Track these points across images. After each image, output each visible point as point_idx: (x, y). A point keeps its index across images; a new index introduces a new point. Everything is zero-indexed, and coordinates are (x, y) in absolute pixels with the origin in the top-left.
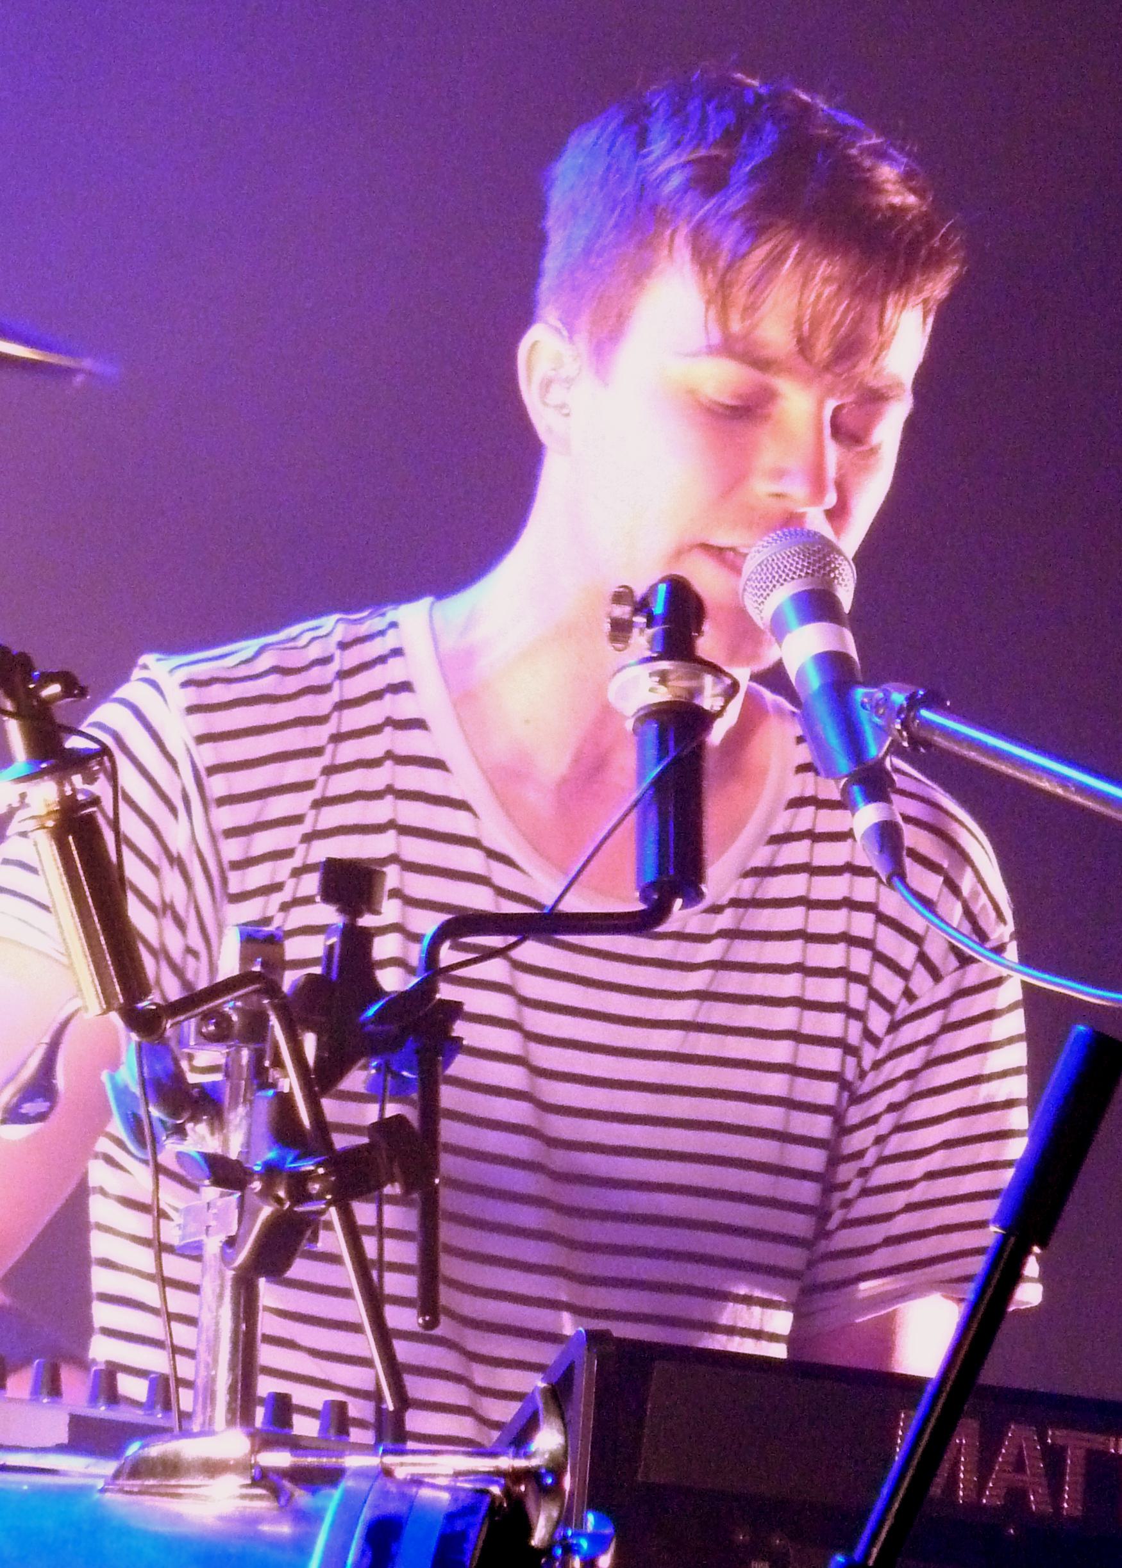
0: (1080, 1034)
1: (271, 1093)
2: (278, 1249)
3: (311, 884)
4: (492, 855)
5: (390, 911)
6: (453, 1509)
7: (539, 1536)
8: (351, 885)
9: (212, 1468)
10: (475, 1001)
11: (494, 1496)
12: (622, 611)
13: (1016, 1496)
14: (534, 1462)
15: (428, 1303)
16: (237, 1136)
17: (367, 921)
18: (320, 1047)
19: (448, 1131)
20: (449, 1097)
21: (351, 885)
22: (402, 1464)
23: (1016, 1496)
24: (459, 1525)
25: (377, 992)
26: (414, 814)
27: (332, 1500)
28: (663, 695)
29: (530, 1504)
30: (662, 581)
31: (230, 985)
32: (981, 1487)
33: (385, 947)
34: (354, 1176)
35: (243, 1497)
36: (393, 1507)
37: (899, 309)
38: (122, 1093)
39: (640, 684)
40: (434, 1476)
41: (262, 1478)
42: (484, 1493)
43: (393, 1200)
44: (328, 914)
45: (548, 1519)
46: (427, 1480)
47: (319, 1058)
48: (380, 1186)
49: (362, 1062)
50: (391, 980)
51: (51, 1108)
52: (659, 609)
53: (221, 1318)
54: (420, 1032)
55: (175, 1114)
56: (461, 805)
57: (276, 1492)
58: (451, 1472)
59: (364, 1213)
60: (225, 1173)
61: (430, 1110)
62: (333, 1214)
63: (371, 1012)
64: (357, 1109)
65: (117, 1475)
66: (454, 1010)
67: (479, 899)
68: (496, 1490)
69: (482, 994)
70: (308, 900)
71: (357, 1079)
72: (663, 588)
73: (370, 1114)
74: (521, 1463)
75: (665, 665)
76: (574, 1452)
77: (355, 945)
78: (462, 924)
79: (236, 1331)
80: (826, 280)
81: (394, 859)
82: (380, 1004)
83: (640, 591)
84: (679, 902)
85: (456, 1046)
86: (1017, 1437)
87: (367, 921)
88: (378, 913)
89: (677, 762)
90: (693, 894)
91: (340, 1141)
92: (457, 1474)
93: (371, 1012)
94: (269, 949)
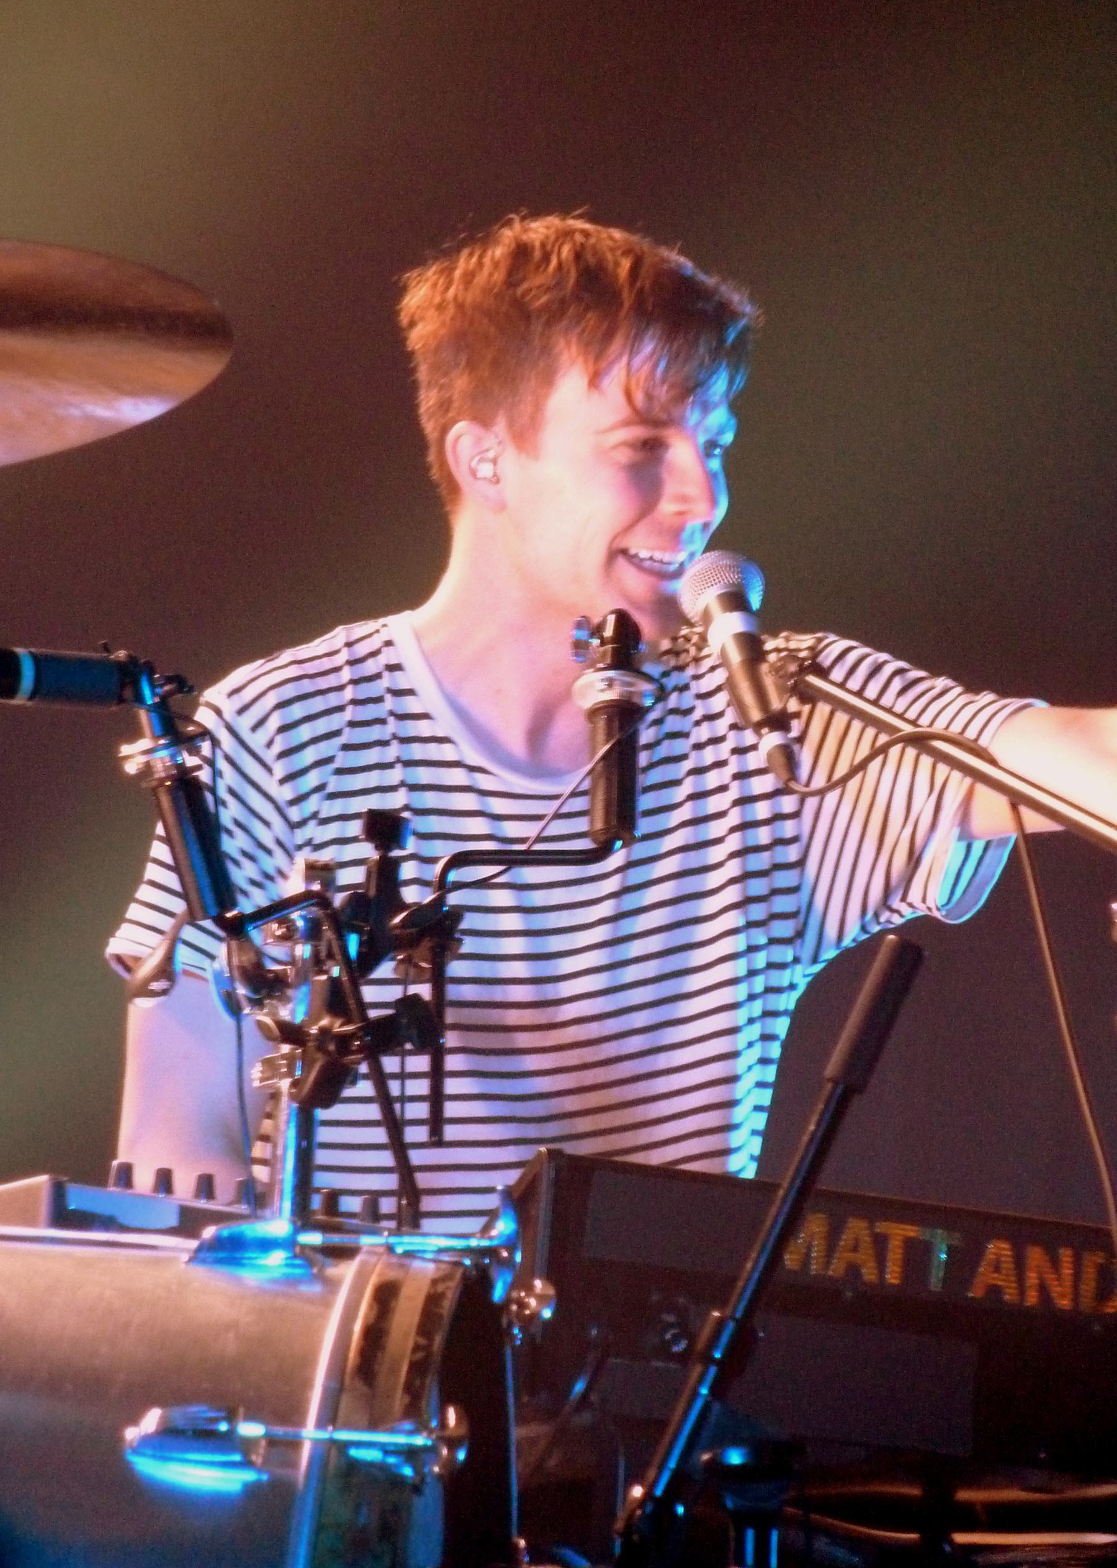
0: (891, 940)
1: (324, 977)
2: (327, 1088)
3: (355, 828)
5: (411, 845)
6: (436, 1276)
7: (498, 1293)
8: (384, 828)
9: (266, 1245)
11: (466, 1267)
12: (582, 635)
13: (853, 1270)
14: (495, 1243)
16: (295, 1009)
17: (396, 853)
18: (361, 944)
21: (384, 828)
22: (400, 1243)
23: (853, 1270)
24: (440, 1288)
25: (402, 906)
27: (347, 1272)
28: (611, 695)
29: (493, 1272)
30: (612, 612)
32: (828, 1264)
33: (408, 871)
34: (383, 1036)
35: (287, 1265)
36: (393, 1275)
37: (630, 342)
39: (596, 687)
40: (424, 1251)
41: (305, 1255)
42: (457, 1264)
43: (411, 1053)
44: (367, 851)
45: (504, 1283)
46: (419, 1255)
47: (360, 954)
48: (402, 1045)
49: (391, 955)
50: (411, 895)
51: (172, 986)
52: (609, 632)
53: (290, 1136)
54: (437, 931)
55: (256, 990)
56: (425, 716)
57: (310, 1263)
58: (436, 1249)
59: (390, 1064)
60: (290, 1033)
63: (397, 920)
65: (199, 1250)
68: (467, 1262)
70: (354, 840)
71: (386, 969)
72: (611, 619)
73: (394, 993)
74: (485, 1243)
75: (611, 673)
77: (386, 873)
79: (298, 1147)
80: (715, 394)
81: (407, 808)
82: (404, 914)
83: (596, 620)
84: (619, 844)
86: (856, 1228)
87: (396, 853)
88: (402, 848)
89: (619, 743)
91: (373, 1014)
92: (441, 1251)
93: (397, 920)
94: (324, 874)
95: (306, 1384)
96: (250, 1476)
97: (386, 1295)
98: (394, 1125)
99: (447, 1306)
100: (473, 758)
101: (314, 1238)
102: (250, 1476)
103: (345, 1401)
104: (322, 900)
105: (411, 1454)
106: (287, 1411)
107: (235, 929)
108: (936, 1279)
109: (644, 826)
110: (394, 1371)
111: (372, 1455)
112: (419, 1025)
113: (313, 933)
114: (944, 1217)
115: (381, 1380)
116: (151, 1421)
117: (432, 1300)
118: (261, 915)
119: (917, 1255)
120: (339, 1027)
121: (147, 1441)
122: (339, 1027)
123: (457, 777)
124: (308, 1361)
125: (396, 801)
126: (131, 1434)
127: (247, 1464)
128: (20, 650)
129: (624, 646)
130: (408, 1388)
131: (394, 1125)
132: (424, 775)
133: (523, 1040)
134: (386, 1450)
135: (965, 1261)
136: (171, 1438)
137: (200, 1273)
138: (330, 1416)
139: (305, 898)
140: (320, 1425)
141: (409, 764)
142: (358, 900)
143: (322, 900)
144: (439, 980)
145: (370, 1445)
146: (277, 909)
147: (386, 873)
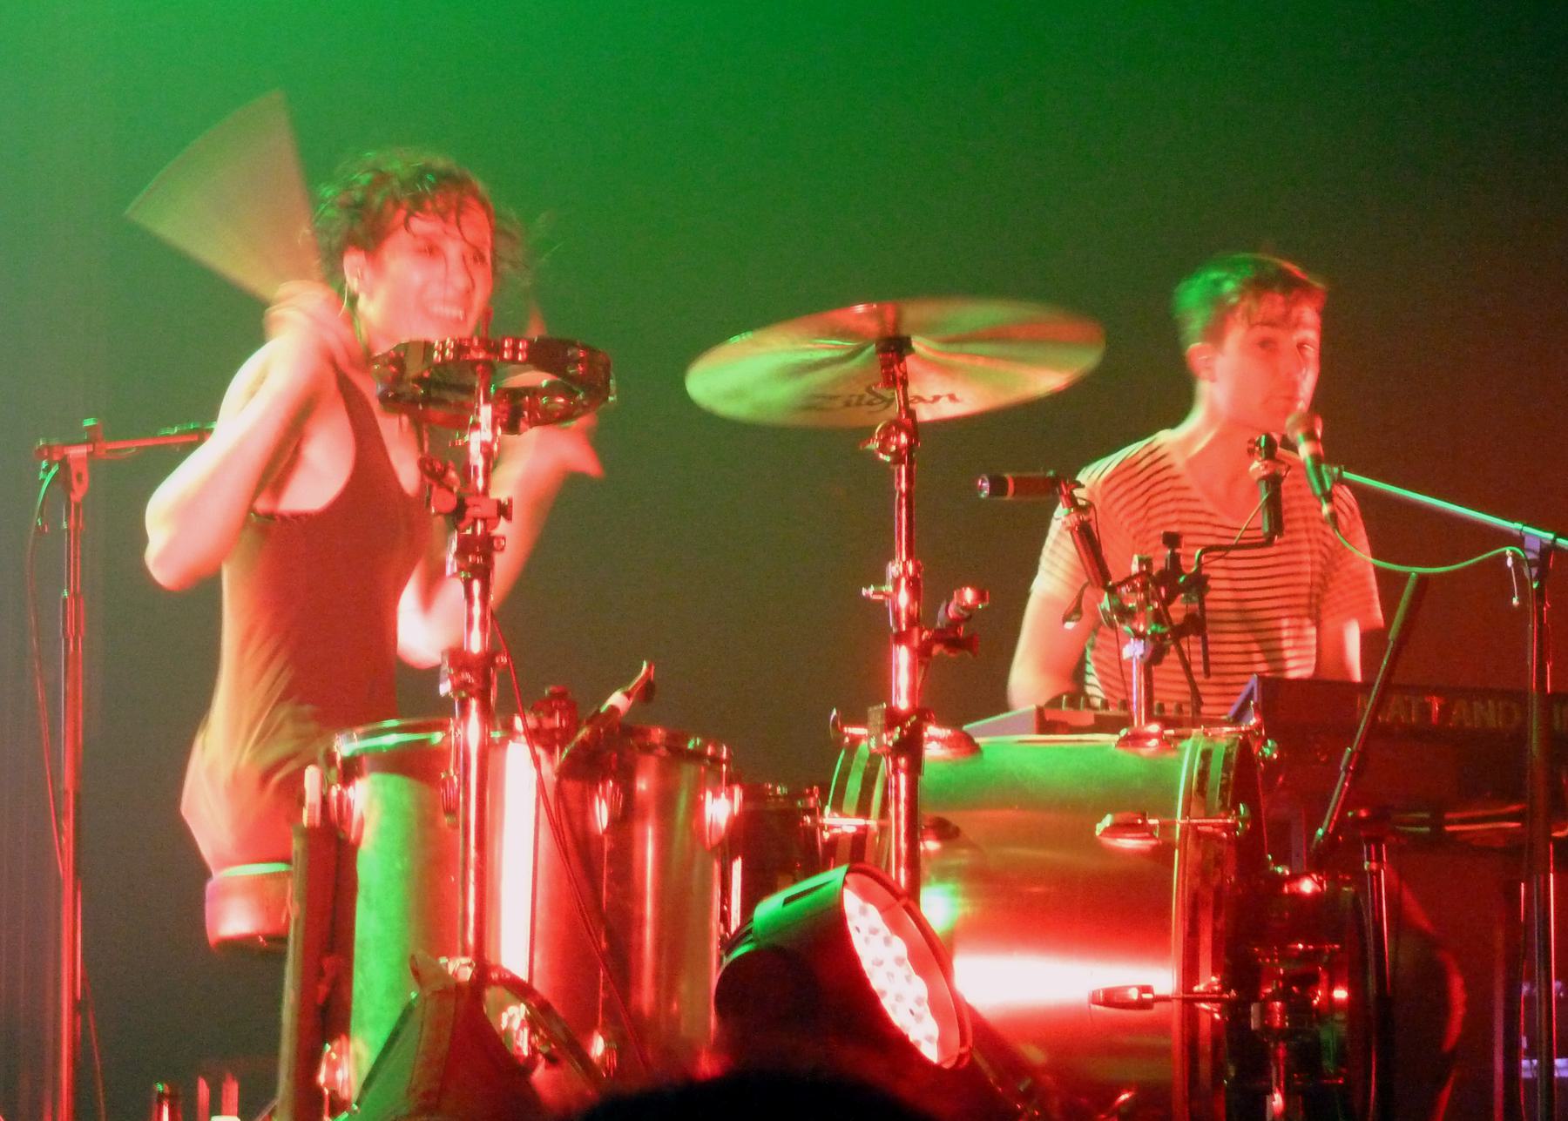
4: (1211, 514)
8: (1172, 540)
10: (1214, 573)
13: (1397, 718)
15: (1207, 673)
19: (1208, 616)
20: (1208, 605)
21: (1172, 540)
23: (1397, 718)
26: (1183, 505)
31: (1137, 576)
34: (1179, 632)
36: (1209, 745)
38: (1104, 611)
54: (1199, 583)
56: (1197, 500)
61: (1202, 609)
62: (1172, 647)
64: (1179, 609)
66: (1207, 577)
67: (1211, 541)
69: (1217, 573)
76: (1143, 1027)
77: (1175, 559)
78: (1208, 549)
85: (1210, 589)
90: (1281, 535)
95: (1176, 798)
96: (1153, 842)
97: (1206, 755)
98: (1187, 666)
99: (1234, 758)
100: (1209, 507)
101: (1171, 732)
102: (1153, 842)
103: (1193, 806)
104: (1148, 573)
105: (1225, 827)
106: (1167, 811)
107: (1112, 591)
108: (1434, 720)
109: (1288, 527)
110: (1214, 790)
111: (1209, 829)
112: (1196, 624)
113: (1144, 588)
114: (1437, 691)
115: (1209, 795)
116: (1108, 820)
117: (1227, 756)
118: (1121, 584)
119: (1425, 711)
120: (1160, 630)
121: (1106, 831)
122: (1160, 630)
123: (1202, 518)
124: (1175, 788)
125: (1175, 529)
126: (1100, 828)
127: (1152, 837)
128: (1007, 475)
129: (1270, 451)
130: (1221, 796)
131: (1187, 666)
132: (1186, 517)
133: (1233, 616)
134: (1213, 826)
135: (1446, 710)
136: (1118, 829)
137: (1121, 752)
138: (1187, 812)
139: (1141, 574)
140: (1183, 817)
141: (1181, 511)
142: (1162, 573)
143: (1148, 573)
144: (1202, 603)
145: (1207, 825)
146: (1128, 580)
147: (1175, 559)
